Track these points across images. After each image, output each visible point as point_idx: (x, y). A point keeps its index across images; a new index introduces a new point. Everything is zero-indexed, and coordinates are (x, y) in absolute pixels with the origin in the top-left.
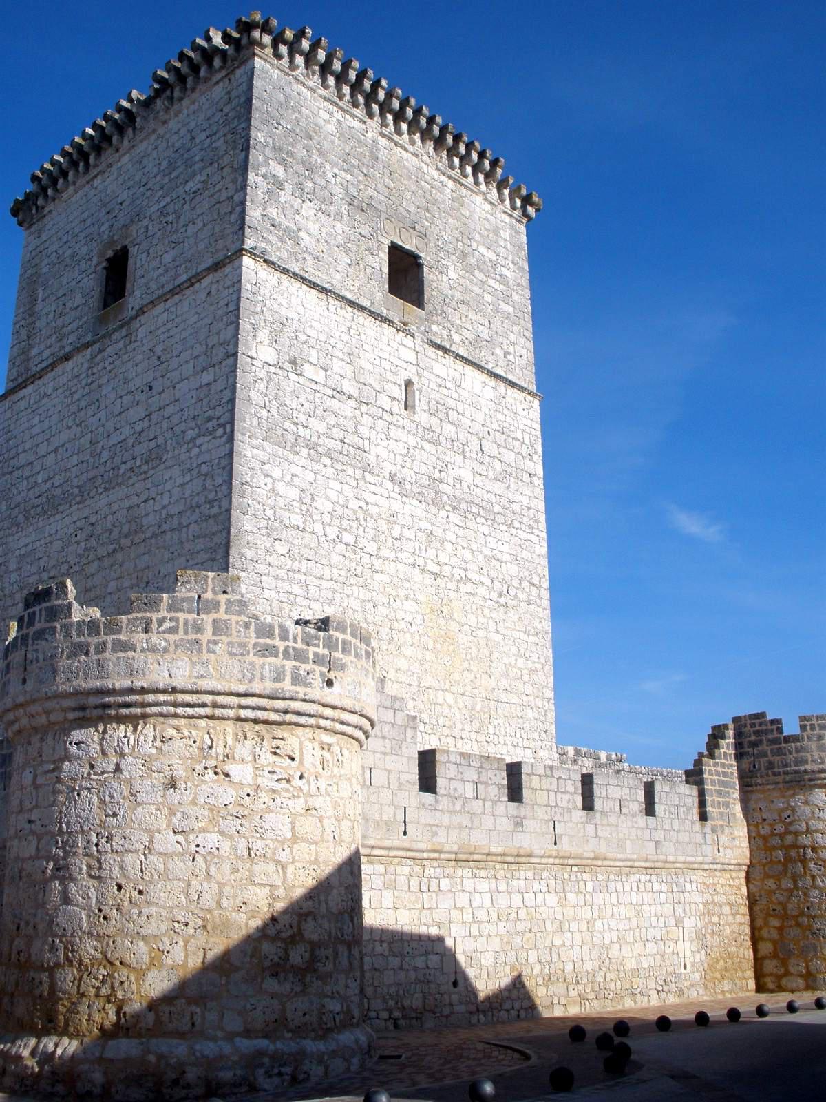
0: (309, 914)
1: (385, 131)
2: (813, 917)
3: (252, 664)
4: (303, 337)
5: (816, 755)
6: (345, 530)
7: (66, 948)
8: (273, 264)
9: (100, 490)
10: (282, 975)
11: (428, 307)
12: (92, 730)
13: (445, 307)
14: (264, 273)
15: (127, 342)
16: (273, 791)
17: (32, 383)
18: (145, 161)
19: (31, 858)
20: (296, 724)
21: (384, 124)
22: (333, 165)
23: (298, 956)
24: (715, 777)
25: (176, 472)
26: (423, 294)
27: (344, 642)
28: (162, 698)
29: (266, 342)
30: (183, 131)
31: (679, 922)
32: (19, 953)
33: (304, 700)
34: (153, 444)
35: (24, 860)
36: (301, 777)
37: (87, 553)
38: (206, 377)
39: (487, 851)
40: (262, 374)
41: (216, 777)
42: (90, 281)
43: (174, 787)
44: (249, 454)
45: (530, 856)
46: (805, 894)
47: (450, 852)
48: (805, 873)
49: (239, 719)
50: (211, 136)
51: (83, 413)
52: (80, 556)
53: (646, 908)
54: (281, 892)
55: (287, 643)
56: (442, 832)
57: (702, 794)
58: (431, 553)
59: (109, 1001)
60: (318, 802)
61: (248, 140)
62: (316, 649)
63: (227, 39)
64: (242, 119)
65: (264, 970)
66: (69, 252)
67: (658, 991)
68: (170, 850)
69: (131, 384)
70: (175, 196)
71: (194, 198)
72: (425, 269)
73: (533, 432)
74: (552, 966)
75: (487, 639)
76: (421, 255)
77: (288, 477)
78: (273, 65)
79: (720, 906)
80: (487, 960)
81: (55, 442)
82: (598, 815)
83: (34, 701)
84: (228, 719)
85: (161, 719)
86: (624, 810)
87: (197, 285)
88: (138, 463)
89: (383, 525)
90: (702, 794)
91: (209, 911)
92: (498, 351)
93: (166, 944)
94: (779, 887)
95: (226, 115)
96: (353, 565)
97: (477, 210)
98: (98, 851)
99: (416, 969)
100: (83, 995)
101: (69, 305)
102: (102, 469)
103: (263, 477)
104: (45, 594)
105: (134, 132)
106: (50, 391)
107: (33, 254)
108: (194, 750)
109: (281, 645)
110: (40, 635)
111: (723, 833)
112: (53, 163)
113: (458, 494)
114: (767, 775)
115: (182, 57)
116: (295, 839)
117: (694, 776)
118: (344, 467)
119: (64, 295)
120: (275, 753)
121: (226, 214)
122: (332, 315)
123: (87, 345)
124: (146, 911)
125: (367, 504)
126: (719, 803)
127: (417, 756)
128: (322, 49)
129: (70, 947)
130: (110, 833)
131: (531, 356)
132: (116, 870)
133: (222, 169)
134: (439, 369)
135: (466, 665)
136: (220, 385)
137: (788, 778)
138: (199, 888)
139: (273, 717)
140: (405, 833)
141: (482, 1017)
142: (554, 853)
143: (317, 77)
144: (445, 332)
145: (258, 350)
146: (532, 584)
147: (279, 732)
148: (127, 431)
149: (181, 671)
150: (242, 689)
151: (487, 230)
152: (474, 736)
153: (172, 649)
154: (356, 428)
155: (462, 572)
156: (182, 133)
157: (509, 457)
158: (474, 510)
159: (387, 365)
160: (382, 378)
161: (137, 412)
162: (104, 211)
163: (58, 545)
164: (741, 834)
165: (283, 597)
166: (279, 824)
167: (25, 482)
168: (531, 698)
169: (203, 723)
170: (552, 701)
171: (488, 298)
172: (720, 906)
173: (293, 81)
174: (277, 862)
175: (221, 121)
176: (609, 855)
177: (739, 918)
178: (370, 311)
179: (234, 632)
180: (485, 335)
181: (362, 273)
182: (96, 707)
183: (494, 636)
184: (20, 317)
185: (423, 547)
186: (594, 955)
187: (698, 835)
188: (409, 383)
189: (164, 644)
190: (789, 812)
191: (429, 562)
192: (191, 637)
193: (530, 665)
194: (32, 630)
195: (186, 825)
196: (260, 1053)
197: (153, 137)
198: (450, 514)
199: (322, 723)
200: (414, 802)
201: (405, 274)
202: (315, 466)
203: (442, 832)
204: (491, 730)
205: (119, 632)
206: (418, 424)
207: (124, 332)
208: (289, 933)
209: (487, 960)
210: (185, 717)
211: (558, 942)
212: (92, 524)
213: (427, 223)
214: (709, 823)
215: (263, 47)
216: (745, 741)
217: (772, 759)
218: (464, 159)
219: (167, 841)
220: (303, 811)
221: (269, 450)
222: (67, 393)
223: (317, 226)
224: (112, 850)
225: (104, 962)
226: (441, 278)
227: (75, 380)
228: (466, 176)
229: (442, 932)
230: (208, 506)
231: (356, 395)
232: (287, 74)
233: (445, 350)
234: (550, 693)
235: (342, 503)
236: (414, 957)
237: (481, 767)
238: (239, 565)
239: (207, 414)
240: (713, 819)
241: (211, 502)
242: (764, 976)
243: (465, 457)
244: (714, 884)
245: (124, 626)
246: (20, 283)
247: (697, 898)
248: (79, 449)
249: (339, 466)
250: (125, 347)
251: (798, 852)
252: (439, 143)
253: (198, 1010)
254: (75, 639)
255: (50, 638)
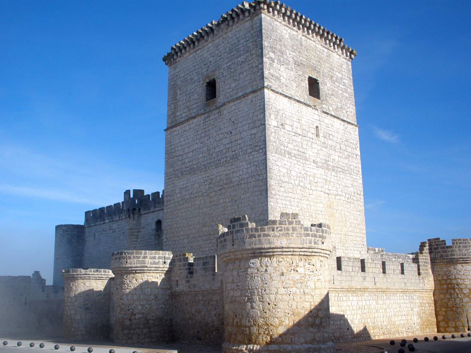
0: (320, 309)
1: (304, 34)
2: (457, 308)
3: (303, 239)
4: (284, 116)
5: (458, 253)
6: (301, 181)
7: (253, 321)
8: (274, 90)
9: (213, 168)
10: (314, 327)
11: (321, 98)
12: (257, 259)
13: (327, 98)
14: (271, 93)
15: (219, 115)
16: (309, 275)
17: (179, 125)
18: (219, 47)
19: (239, 296)
20: (314, 255)
21: (304, 32)
22: (289, 50)
23: (317, 321)
24: (423, 260)
25: (244, 163)
26: (320, 94)
27: (326, 230)
28: (279, 250)
29: (274, 119)
30: (234, 38)
31: (412, 309)
32: (237, 323)
33: (317, 249)
34: (234, 153)
35: (236, 297)
36: (316, 271)
37: (210, 189)
38: (254, 131)
39: (356, 288)
40: (273, 130)
41: (294, 272)
42: (201, 90)
43: (283, 275)
44: (271, 159)
45: (368, 289)
46: (454, 300)
47: (345, 289)
48: (454, 293)
49: (300, 255)
50: (246, 41)
51: (203, 139)
52: (208, 190)
53: (402, 305)
54: (313, 304)
55: (312, 232)
56: (343, 282)
57: (419, 266)
58: (327, 187)
59: (268, 335)
60: (320, 277)
61: (262, 45)
62: (319, 233)
63: (251, 7)
64: (259, 37)
65: (309, 325)
66: (189, 78)
67: (406, 332)
68: (283, 293)
69: (223, 130)
70: (233, 63)
71: (242, 64)
72: (320, 84)
73: (356, 139)
74: (375, 323)
75: (345, 215)
76: (318, 79)
77: (283, 165)
78: (268, 16)
79: (425, 304)
80: (356, 322)
81: (192, 148)
82: (387, 275)
83: (237, 251)
84: (297, 255)
85: (278, 256)
86: (395, 273)
87: (247, 97)
88: (229, 159)
89: (312, 178)
90: (419, 266)
91: (294, 309)
92: (344, 111)
93: (283, 319)
94: (445, 298)
95: (252, 34)
96: (304, 193)
97: (335, 58)
98: (262, 294)
99: (337, 325)
100: (260, 334)
101: (192, 98)
102: (213, 160)
103: (276, 166)
104: (239, 219)
105: (213, 36)
106: (187, 129)
107: (173, 76)
108: (288, 265)
109: (311, 233)
110: (238, 231)
111: (425, 279)
112: (180, 43)
113: (334, 165)
114: (441, 259)
115: (233, 11)
116: (315, 288)
117: (416, 260)
118: (299, 160)
119: (189, 94)
120: (309, 264)
121: (256, 72)
122: (293, 106)
123: (202, 114)
124: (277, 310)
125: (307, 171)
126: (424, 269)
127: (336, 259)
128: (284, 8)
129: (255, 321)
130: (265, 289)
131: (355, 111)
132: (268, 299)
133: (252, 54)
134: (326, 121)
135: (338, 224)
136: (259, 134)
137: (448, 260)
138: (291, 303)
139: (309, 254)
140: (334, 283)
141: (355, 339)
142: (375, 288)
143: (281, 18)
144: (327, 107)
145: (271, 122)
146: (358, 194)
147: (310, 258)
148: (222, 147)
149: (283, 242)
150: (301, 246)
151: (339, 66)
152: (341, 248)
153: (281, 236)
154: (302, 145)
155: (336, 192)
156: (234, 38)
157: (349, 149)
158: (339, 170)
159: (310, 122)
160: (309, 127)
161: (227, 141)
162: (203, 64)
163: (197, 185)
164: (432, 279)
165: (284, 206)
166: (311, 284)
167: (180, 162)
168: (359, 234)
169: (290, 257)
170: (365, 234)
171: (340, 92)
172: (425, 304)
173: (274, 20)
174: (311, 295)
175: (250, 36)
176: (391, 288)
177: (431, 308)
178: (304, 103)
179: (298, 231)
180: (340, 106)
181: (300, 89)
182: (258, 253)
183: (347, 213)
184: (170, 100)
185: (324, 185)
186: (387, 320)
187: (418, 280)
188: (317, 127)
189: (278, 234)
190: (448, 272)
191: (326, 190)
192: (286, 232)
193: (358, 222)
194: (234, 230)
195: (287, 286)
196: (310, 348)
197: (222, 38)
198: (332, 172)
199: (321, 254)
200: (336, 274)
201: (314, 87)
202: (291, 160)
203: (343, 282)
204: (347, 245)
205: (265, 231)
206: (321, 141)
207: (217, 111)
208: (315, 315)
209: (356, 322)
210: (285, 255)
211: (376, 316)
212: (211, 179)
213: (319, 67)
214: (421, 276)
215: (264, 10)
216: (433, 248)
217: (442, 254)
218: (330, 41)
219: (282, 291)
220: (317, 280)
221: (277, 157)
222: (195, 131)
223: (285, 74)
224: (266, 294)
225: (266, 325)
226: (324, 88)
227: (198, 127)
228: (331, 47)
229: (344, 313)
230: (258, 176)
231: (301, 134)
232: (272, 18)
233: (328, 114)
234: (364, 232)
235: (299, 172)
236: (337, 321)
237: (354, 261)
238: (271, 196)
239: (255, 144)
240: (422, 275)
241: (259, 175)
242: (440, 327)
243: (335, 151)
244: (423, 297)
245: (266, 229)
246: (169, 87)
247: (417, 301)
248: (202, 152)
249: (298, 160)
250: (219, 117)
251: (452, 286)
252: (322, 36)
253: (293, 337)
254: (250, 233)
255: (242, 233)
